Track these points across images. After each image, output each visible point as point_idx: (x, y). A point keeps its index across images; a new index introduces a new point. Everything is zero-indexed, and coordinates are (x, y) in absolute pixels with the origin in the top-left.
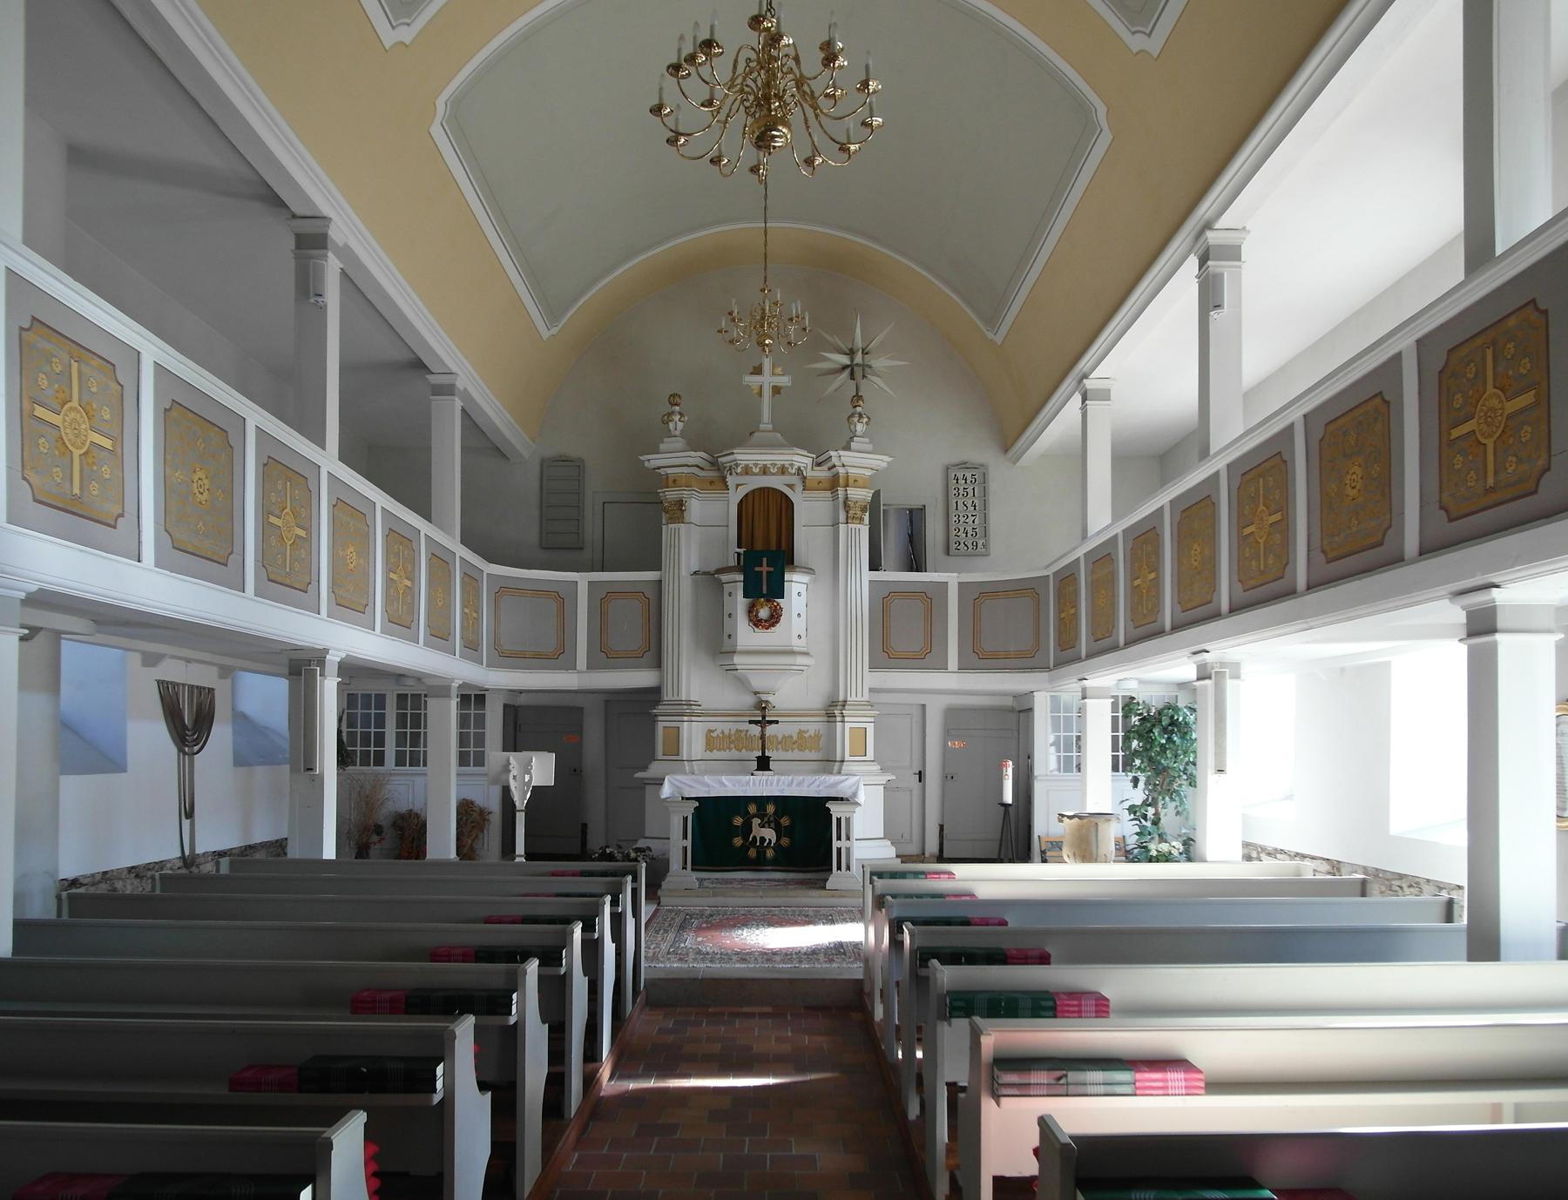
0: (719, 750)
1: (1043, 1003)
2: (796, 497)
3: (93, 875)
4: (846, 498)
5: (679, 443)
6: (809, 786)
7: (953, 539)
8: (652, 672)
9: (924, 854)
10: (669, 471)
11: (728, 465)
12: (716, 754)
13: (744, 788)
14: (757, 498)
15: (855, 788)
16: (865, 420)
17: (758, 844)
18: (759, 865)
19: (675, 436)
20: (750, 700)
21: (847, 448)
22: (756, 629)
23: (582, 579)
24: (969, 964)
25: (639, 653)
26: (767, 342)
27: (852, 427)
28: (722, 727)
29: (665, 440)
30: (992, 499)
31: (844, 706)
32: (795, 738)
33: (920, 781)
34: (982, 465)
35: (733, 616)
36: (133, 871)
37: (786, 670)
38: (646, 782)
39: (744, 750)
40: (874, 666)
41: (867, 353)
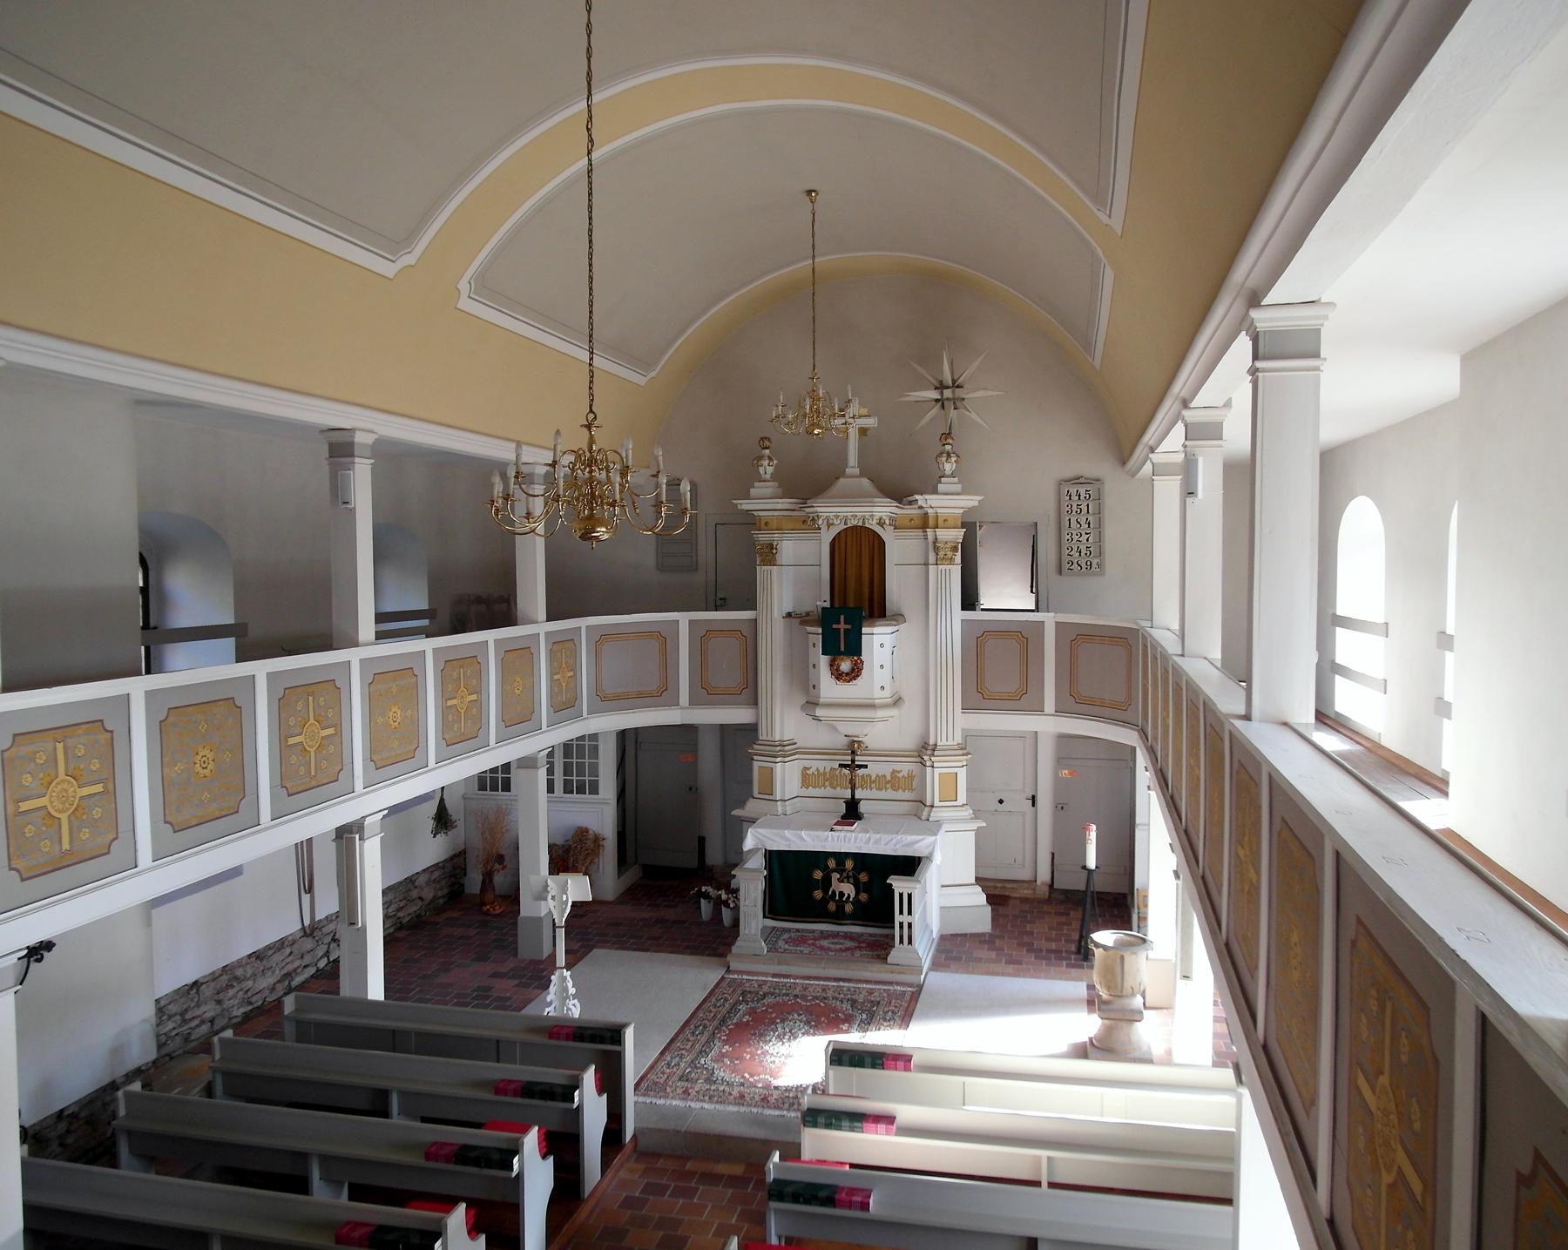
0: (814, 787)
2: (887, 535)
3: (213, 973)
5: (767, 488)
7: (1066, 559)
8: (750, 710)
9: (1036, 881)
10: (755, 513)
11: (811, 515)
12: (811, 791)
13: (823, 844)
15: (931, 848)
16: (953, 459)
17: (837, 898)
18: (839, 919)
19: (765, 481)
21: (935, 491)
23: (683, 619)
26: (816, 432)
29: (756, 484)
30: (1107, 514)
31: (934, 750)
32: (889, 778)
33: (1033, 805)
34: (1098, 480)
35: (817, 667)
37: (871, 721)
40: (966, 707)
41: (958, 387)
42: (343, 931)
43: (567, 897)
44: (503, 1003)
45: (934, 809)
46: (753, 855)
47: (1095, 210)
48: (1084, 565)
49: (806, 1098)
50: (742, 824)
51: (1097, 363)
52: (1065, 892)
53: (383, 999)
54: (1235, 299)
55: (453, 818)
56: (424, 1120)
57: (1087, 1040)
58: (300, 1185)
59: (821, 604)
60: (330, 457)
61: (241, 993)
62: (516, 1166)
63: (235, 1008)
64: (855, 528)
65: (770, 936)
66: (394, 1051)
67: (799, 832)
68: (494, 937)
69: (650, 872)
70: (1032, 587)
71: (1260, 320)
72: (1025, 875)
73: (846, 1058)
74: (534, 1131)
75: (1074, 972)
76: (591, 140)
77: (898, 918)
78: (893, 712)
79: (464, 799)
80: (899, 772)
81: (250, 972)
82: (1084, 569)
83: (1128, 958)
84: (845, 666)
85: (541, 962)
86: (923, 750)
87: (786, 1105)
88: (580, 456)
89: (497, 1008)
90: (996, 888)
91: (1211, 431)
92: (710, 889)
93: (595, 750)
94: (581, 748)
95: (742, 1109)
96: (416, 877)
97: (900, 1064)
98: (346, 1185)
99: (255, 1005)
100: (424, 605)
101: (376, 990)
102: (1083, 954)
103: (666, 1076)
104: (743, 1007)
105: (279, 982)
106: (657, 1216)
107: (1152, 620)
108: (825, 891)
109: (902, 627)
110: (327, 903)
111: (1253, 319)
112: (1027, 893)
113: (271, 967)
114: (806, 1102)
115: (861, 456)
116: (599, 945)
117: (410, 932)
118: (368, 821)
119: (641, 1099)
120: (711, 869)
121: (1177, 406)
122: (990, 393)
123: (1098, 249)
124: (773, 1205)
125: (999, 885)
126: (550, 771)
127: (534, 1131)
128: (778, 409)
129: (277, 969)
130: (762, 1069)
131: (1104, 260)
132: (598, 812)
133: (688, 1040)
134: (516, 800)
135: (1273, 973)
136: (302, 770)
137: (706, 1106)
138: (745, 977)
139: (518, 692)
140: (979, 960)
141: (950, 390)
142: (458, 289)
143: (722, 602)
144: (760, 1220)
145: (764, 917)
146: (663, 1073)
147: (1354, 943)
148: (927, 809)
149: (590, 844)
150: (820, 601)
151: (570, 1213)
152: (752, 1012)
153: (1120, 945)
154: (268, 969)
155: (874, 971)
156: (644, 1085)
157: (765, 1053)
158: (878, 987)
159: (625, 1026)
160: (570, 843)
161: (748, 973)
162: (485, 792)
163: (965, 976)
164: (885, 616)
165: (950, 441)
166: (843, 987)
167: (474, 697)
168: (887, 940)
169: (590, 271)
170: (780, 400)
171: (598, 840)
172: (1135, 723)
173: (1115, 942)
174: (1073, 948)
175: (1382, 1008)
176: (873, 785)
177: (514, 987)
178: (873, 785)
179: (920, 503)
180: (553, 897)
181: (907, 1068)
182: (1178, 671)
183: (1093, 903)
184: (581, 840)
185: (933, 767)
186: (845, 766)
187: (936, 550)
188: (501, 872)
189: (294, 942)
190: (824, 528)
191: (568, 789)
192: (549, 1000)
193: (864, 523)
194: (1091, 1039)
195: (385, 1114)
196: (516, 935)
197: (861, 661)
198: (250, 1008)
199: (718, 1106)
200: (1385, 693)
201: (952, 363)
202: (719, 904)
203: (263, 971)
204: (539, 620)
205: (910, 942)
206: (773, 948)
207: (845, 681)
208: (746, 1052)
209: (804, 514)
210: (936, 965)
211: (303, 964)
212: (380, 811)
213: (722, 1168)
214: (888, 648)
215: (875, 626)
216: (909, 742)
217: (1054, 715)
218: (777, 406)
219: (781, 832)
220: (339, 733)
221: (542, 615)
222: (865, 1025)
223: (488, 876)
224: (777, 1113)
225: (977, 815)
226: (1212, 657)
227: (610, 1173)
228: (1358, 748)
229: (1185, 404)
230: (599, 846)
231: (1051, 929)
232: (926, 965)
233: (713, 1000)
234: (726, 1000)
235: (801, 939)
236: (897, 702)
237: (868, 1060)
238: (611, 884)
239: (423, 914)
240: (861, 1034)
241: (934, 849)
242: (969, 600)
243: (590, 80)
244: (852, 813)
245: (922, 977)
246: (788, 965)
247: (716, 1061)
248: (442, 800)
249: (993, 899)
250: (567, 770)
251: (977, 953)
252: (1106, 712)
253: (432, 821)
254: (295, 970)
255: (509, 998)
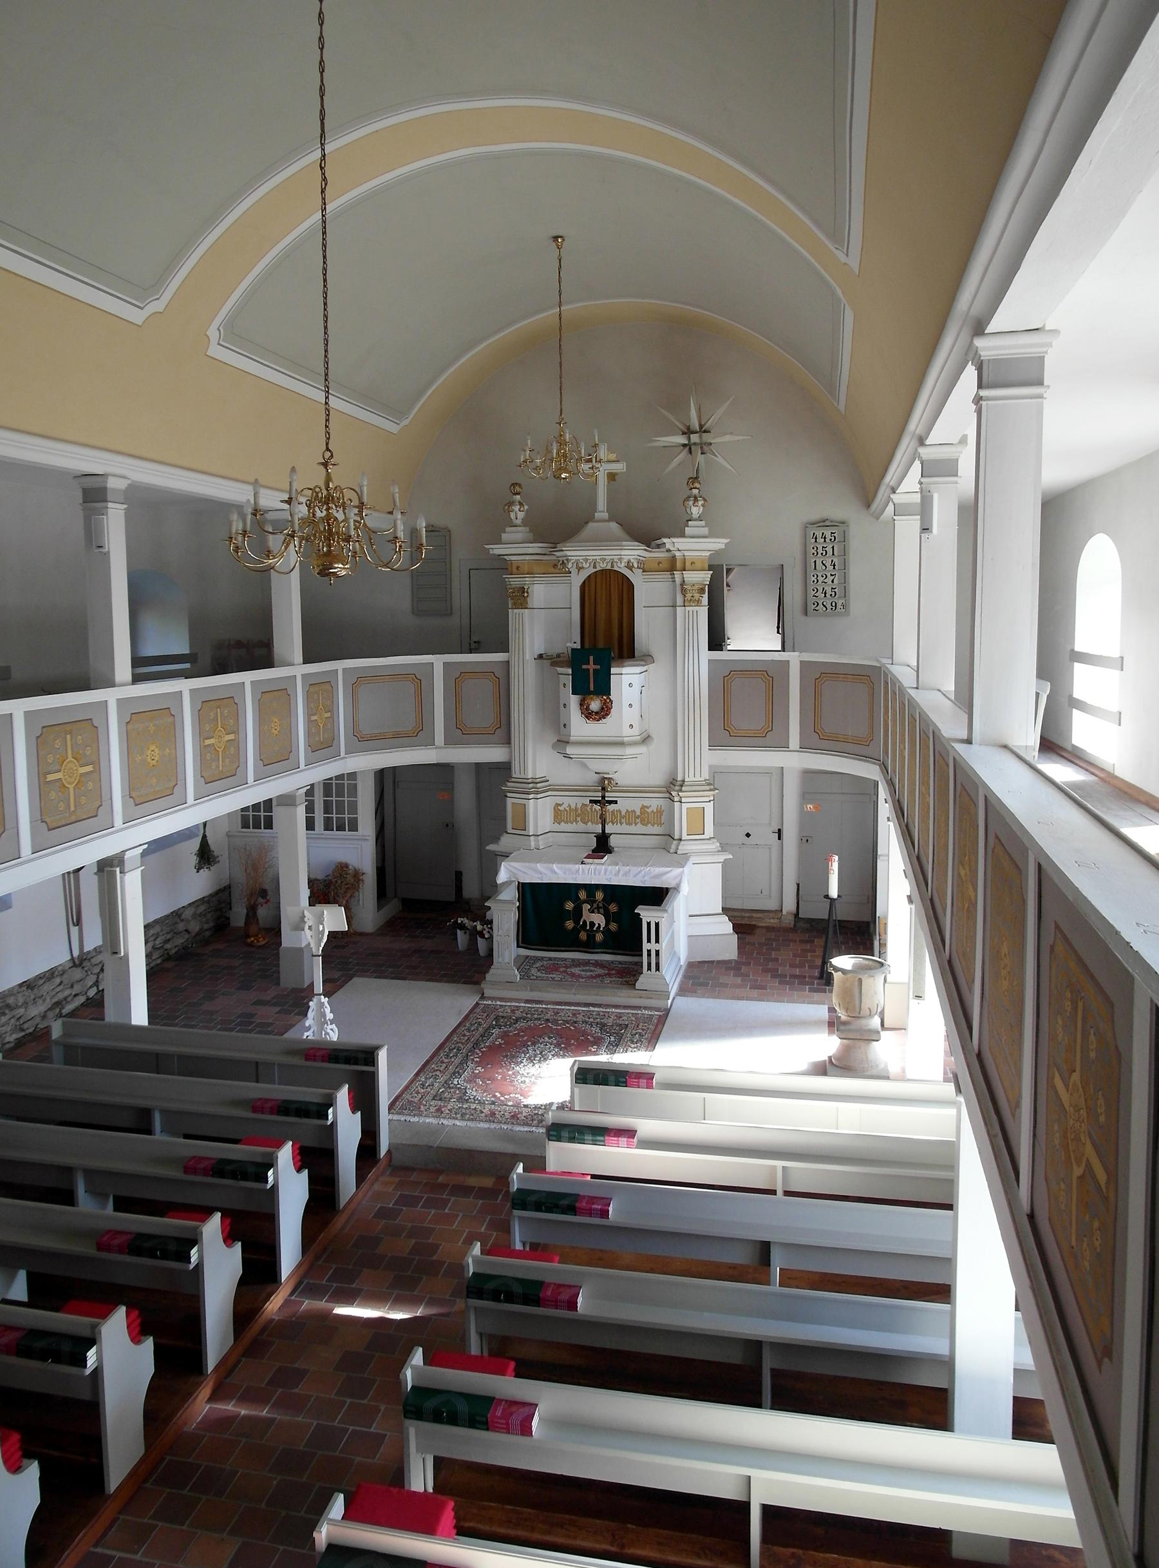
1: (478, 1418)
2: (636, 578)
4: (683, 583)
5: (520, 533)
6: (635, 876)
7: (811, 600)
8: (503, 749)
9: (782, 910)
12: (564, 827)
13: (574, 876)
14: (599, 579)
15: (678, 880)
16: (700, 503)
17: (588, 928)
20: (593, 779)
21: (683, 535)
22: (588, 721)
23: (437, 661)
24: (508, 1303)
25: (491, 730)
27: (688, 510)
28: (570, 801)
29: (508, 529)
30: (852, 557)
31: (682, 786)
32: (638, 813)
33: (779, 838)
35: (567, 707)
36: (24, 984)
37: (620, 758)
38: (497, 853)
39: (590, 823)
40: (713, 745)
41: (705, 431)
42: (105, 957)
43: (323, 927)
44: (264, 1028)
45: (682, 843)
46: (507, 886)
47: (832, 248)
48: (829, 607)
49: (550, 1113)
50: (497, 858)
51: (842, 407)
52: (810, 921)
53: (147, 1024)
54: (960, 330)
55: (215, 853)
56: (186, 1136)
57: (827, 1059)
58: (67, 1197)
59: (571, 645)
60: (84, 502)
61: (13, 1021)
62: (271, 1179)
63: (8, 1034)
64: (603, 571)
65: (523, 965)
66: (158, 1073)
67: (551, 865)
68: (257, 968)
69: (408, 904)
70: (778, 628)
71: (985, 349)
72: (772, 905)
73: (590, 1077)
74: (289, 1146)
75: (817, 996)
76: (325, 179)
77: (646, 946)
78: (642, 749)
79: (228, 836)
80: (648, 808)
81: (21, 1000)
82: (829, 610)
83: (867, 982)
84: (595, 705)
85: (303, 990)
86: (672, 786)
87: (535, 1122)
88: (317, 493)
89: (260, 1032)
90: (743, 917)
91: (945, 468)
92: (466, 921)
93: (353, 790)
94: (340, 788)
95: (493, 1126)
96: (182, 911)
97: (643, 1082)
98: (111, 1197)
99: (27, 1032)
100: (186, 650)
101: (139, 1015)
102: (825, 979)
103: (420, 1096)
104: (496, 1031)
105: (50, 1009)
106: (410, 1224)
107: (892, 658)
108: (577, 922)
109: (651, 667)
110: (93, 938)
111: (977, 347)
112: (773, 922)
113: (43, 995)
114: (550, 1117)
115: (611, 501)
116: (358, 974)
117: (176, 963)
118: (128, 855)
119: (396, 1117)
120: (468, 902)
121: (914, 443)
122: (737, 438)
123: (837, 288)
124: (516, 1212)
125: (747, 915)
126: (310, 809)
127: (289, 1146)
128: (525, 455)
129: (48, 998)
130: (512, 1088)
131: (844, 300)
132: (357, 848)
133: (443, 1062)
134: (276, 837)
135: (986, 980)
136: (62, 807)
137: (458, 1123)
138: (498, 1003)
139: (276, 732)
140: (725, 985)
141: (698, 434)
142: (207, 335)
143: (476, 645)
144: (505, 1228)
145: (518, 946)
146: (418, 1093)
147: (1052, 948)
148: (675, 842)
149: (350, 879)
150: (571, 642)
151: (326, 1224)
152: (504, 1035)
153: (858, 969)
154: (39, 997)
155: (623, 996)
156: (399, 1104)
157: (516, 1074)
158: (626, 1011)
159: (378, 1048)
160: (330, 878)
161: (501, 999)
162: (249, 830)
163: (711, 1000)
164: (634, 657)
165: (697, 485)
166: (593, 1011)
167: (232, 737)
168: (636, 968)
169: (325, 310)
170: (527, 444)
171: (358, 875)
172: (878, 758)
173: (854, 965)
174: (817, 973)
175: (1075, 1009)
176: (623, 820)
177: (275, 1013)
178: (623, 820)
179: (668, 546)
180: (310, 928)
181: (649, 1086)
182: (913, 704)
183: (835, 932)
184: (341, 875)
185: (681, 802)
186: (596, 802)
187: (684, 592)
188: (264, 905)
189: (63, 972)
190: (574, 571)
191: (328, 827)
192: (307, 1025)
193: (612, 566)
194: (830, 1058)
195: (149, 1131)
196: (278, 966)
197: (610, 700)
198: (23, 1034)
199: (469, 1123)
200: (1120, 725)
201: (700, 409)
202: (474, 934)
203: (34, 999)
204: (296, 662)
205: (658, 969)
206: (525, 976)
207: (594, 719)
208: (498, 1073)
209: (554, 558)
210: (683, 991)
211: (74, 994)
212: (140, 845)
213: (473, 1181)
214: (636, 688)
215: (623, 667)
216: (657, 778)
217: (798, 751)
218: (525, 451)
219: (532, 865)
220: (97, 770)
221: (298, 656)
222: (613, 1047)
223: (252, 910)
224: (526, 1129)
225: (724, 848)
226: (946, 689)
227: (365, 1186)
228: (1093, 778)
229: (921, 442)
230: (359, 880)
231: (795, 955)
232: (673, 991)
233: (467, 1025)
234: (480, 1024)
235: (553, 967)
236: (646, 739)
237: (612, 1078)
238: (370, 915)
239: (190, 946)
240: (609, 1056)
241: (681, 880)
242: (717, 641)
243: (323, 119)
244: (603, 847)
245: (670, 1002)
246: (540, 991)
247: (469, 1081)
248: (204, 837)
249: (737, 928)
250: (327, 808)
251: (723, 979)
252: (850, 747)
253: (196, 857)
254: (65, 999)
255: (272, 1024)
